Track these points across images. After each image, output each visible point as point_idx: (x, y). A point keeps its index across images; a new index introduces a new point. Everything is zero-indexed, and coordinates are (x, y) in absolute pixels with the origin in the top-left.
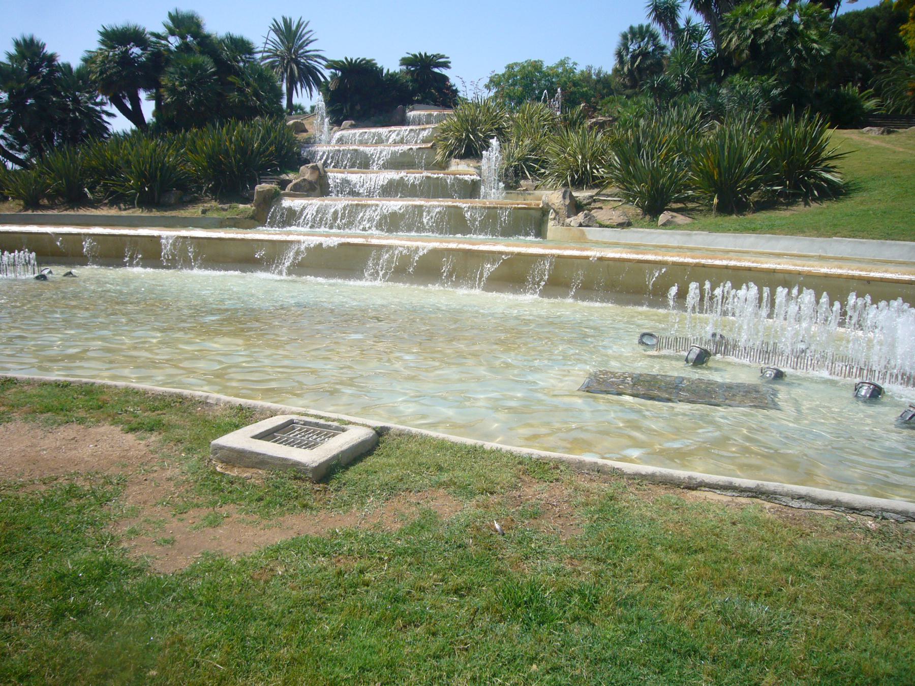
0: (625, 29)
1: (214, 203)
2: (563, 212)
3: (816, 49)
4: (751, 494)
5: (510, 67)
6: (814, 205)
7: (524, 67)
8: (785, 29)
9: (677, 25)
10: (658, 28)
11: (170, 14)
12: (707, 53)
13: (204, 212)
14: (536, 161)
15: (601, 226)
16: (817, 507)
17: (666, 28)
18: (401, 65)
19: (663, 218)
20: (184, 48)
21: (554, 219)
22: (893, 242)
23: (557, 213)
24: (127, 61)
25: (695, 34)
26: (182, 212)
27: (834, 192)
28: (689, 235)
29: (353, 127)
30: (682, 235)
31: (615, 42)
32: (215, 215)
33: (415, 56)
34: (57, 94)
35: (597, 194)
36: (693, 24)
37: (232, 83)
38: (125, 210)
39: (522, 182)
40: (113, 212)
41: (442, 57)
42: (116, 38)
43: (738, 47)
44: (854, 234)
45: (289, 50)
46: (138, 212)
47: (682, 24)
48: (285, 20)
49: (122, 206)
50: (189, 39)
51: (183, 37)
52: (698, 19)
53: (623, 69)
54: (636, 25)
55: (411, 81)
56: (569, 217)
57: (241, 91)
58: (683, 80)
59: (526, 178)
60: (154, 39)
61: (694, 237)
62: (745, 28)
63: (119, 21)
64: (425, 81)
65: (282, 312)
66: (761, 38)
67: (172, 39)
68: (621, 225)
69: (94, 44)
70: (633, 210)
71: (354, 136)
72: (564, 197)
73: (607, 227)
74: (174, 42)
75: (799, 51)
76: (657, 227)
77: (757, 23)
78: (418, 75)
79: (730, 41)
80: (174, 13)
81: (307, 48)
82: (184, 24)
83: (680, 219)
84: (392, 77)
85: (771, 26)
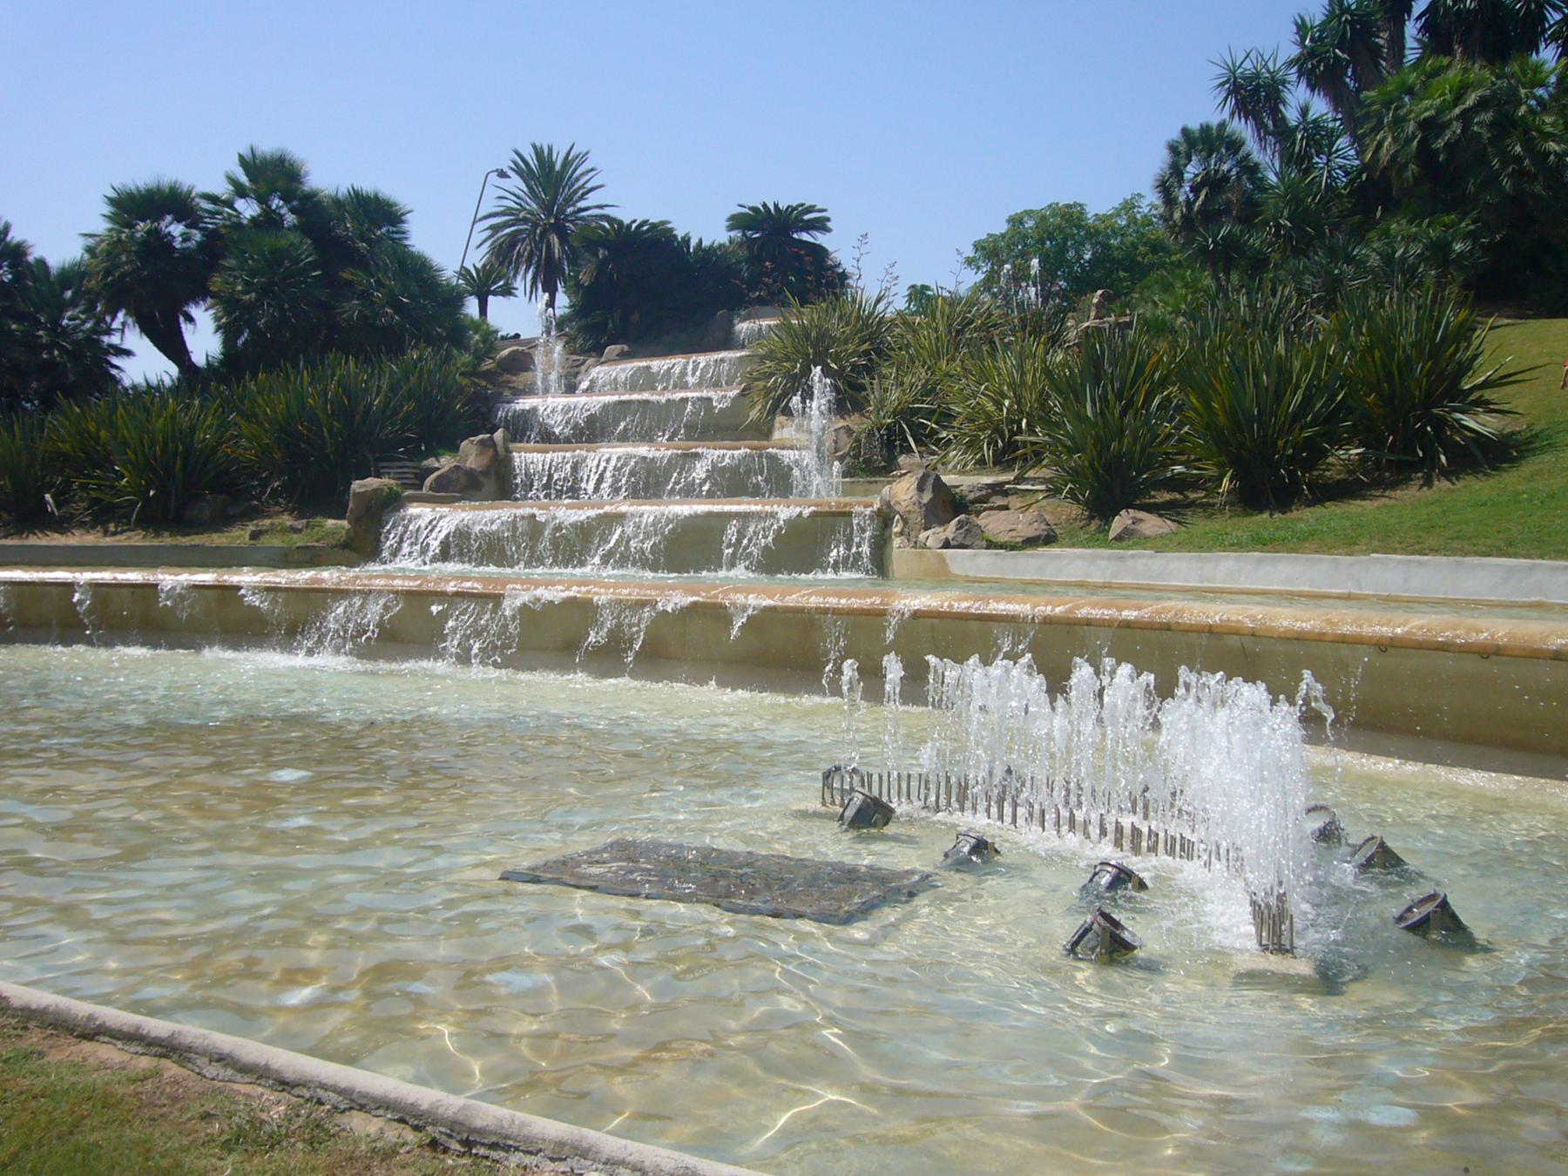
0: (1175, 134)
1: (287, 520)
2: (917, 518)
3: (1556, 154)
4: (160, 1050)
5: (1016, 221)
6: (1441, 485)
7: (1044, 218)
8: (1487, 117)
9: (1284, 119)
10: (1243, 129)
11: (241, 157)
12: (1347, 174)
13: (255, 536)
14: (929, 414)
15: (991, 545)
16: (238, 1077)
17: (1260, 125)
18: (730, 228)
19: (1120, 522)
20: (269, 221)
21: (901, 533)
22: (1477, 560)
23: (905, 521)
24: (156, 255)
25: (1319, 137)
26: (215, 536)
27: (1495, 454)
28: (1122, 558)
29: (624, 356)
30: (1109, 558)
31: (1159, 161)
32: (276, 542)
33: (754, 209)
34: (19, 317)
35: (1018, 480)
36: (1311, 116)
37: (350, 284)
38: (115, 534)
39: (902, 459)
40: (91, 539)
41: (811, 209)
42: (135, 207)
43: (1393, 158)
44: (1416, 547)
45: (547, 208)
46: (136, 539)
47: (1292, 115)
48: (538, 152)
49: (112, 527)
50: (276, 203)
51: (262, 200)
52: (1320, 107)
53: (1171, 215)
54: (1194, 126)
55: (747, 260)
56: (926, 529)
57: (365, 296)
58: (1277, 231)
59: (909, 450)
60: (210, 206)
61: (1130, 563)
62: (1404, 119)
63: (141, 175)
64: (781, 255)
65: (471, 740)
66: (1438, 136)
67: (240, 204)
68: (1031, 542)
69: (98, 223)
70: (1067, 510)
71: (610, 378)
72: (921, 488)
73: (1001, 546)
74: (248, 209)
75: (1518, 159)
76: (1106, 544)
77: (1426, 107)
78: (761, 248)
79: (1380, 145)
80: (247, 153)
81: (582, 204)
82: (271, 175)
83: (1152, 524)
84: (708, 256)
85: (1457, 111)
